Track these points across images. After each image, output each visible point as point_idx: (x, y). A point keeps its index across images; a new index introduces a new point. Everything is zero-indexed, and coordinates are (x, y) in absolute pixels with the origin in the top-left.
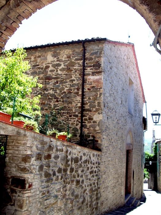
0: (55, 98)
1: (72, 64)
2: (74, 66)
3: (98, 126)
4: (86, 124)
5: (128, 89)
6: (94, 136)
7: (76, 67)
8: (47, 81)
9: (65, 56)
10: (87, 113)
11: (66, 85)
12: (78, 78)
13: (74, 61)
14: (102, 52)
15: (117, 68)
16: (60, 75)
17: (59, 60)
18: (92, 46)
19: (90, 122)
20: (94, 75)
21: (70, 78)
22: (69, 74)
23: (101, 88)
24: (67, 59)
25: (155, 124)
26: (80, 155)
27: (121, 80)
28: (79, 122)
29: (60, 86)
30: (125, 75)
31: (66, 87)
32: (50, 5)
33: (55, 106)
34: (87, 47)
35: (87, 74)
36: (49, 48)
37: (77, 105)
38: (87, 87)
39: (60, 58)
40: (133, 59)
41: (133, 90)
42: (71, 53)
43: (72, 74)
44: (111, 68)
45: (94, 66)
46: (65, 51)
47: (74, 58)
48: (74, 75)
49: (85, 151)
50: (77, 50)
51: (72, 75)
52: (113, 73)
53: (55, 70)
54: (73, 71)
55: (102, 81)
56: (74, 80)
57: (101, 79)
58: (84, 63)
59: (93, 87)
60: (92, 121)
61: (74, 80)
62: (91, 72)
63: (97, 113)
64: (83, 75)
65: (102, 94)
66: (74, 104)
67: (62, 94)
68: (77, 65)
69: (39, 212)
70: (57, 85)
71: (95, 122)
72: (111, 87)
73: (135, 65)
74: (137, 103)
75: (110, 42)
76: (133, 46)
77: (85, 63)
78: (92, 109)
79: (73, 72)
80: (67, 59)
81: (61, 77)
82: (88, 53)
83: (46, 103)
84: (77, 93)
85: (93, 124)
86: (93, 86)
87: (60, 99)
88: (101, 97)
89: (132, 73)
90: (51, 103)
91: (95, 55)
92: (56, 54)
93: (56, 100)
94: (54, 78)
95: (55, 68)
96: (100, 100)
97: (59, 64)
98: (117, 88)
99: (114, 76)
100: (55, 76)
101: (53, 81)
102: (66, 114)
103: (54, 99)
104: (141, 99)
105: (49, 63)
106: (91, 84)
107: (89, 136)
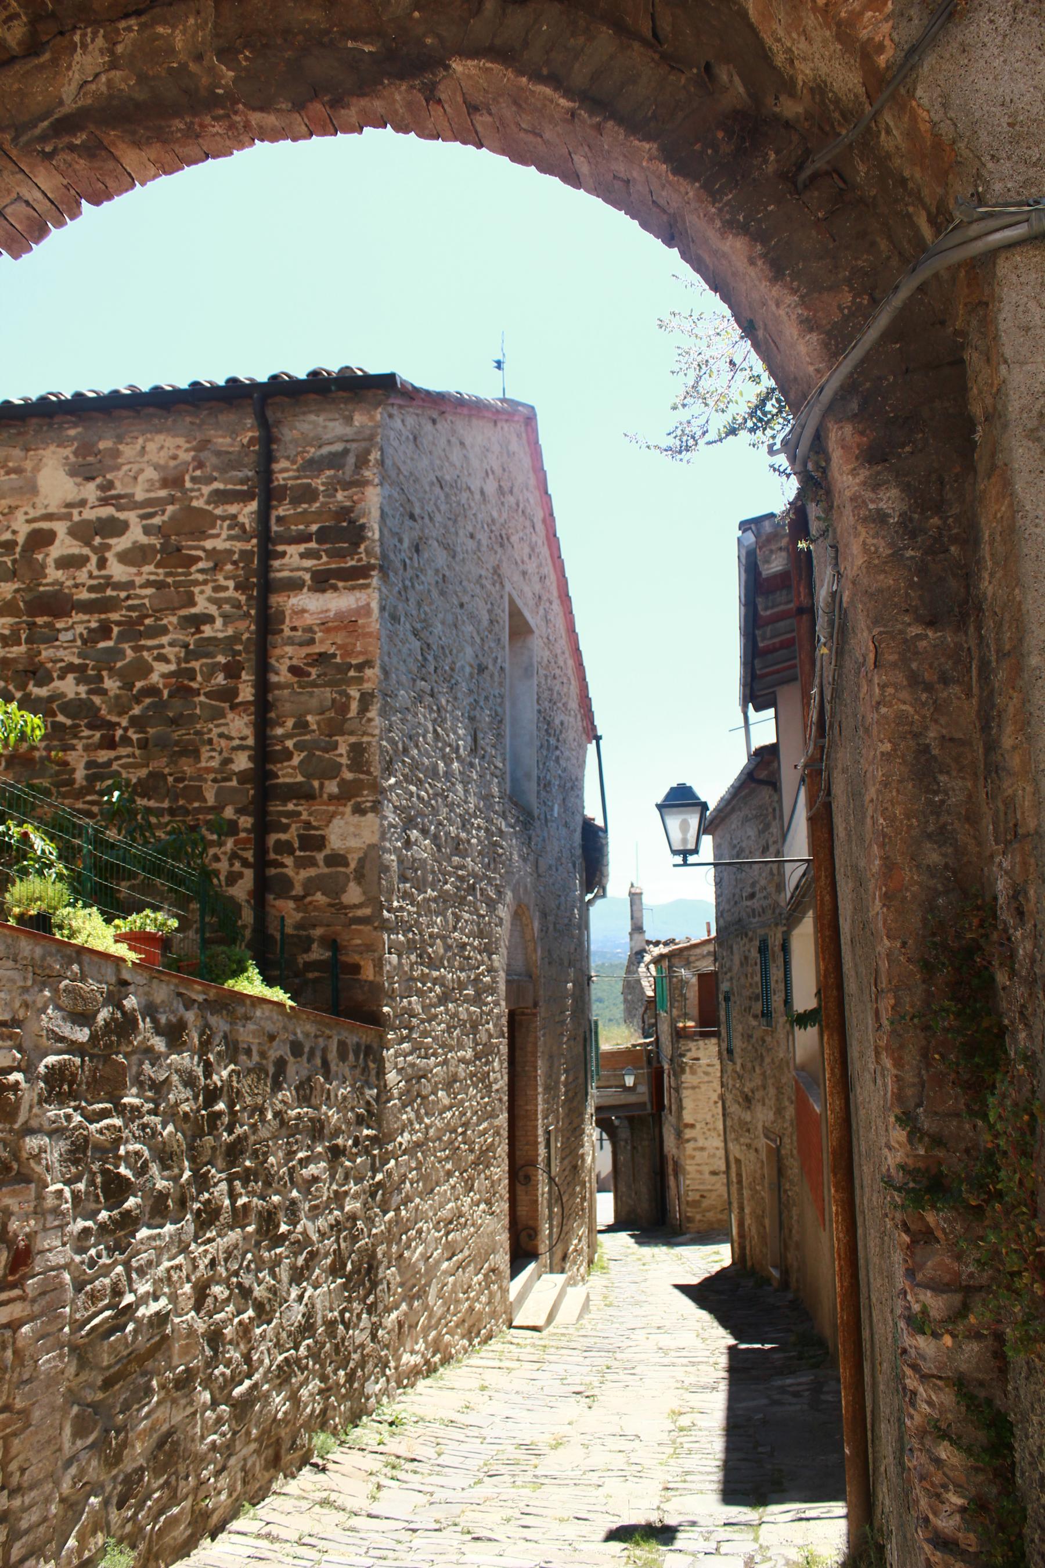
0: (90, 727)
1: (197, 524)
2: (204, 535)
3: (359, 883)
4: (285, 875)
5: (507, 666)
6: (335, 941)
7: (219, 541)
8: (40, 621)
9: (150, 473)
10: (290, 807)
11: (162, 646)
12: (233, 607)
13: (208, 503)
14: (368, 452)
15: (447, 547)
16: (118, 586)
17: (113, 497)
18: (312, 417)
19: (312, 863)
20: (323, 591)
21: (180, 608)
22: (177, 584)
23: (368, 664)
24: (163, 493)
25: (679, 859)
26: (273, 1054)
27: (471, 616)
28: (245, 863)
29: (122, 653)
30: (488, 584)
31: (163, 658)
32: (164, 181)
33: (97, 772)
34: (278, 422)
35: (281, 579)
36: (50, 425)
37: (227, 761)
38: (286, 656)
39: (117, 484)
40: (527, 494)
41: (528, 672)
42: (186, 456)
43: (196, 583)
44: (417, 550)
45: (322, 536)
46: (151, 447)
47: (206, 490)
48: (208, 589)
49: (299, 1031)
50: (222, 441)
51: (196, 590)
52: (430, 572)
53: (87, 559)
54: (201, 565)
55: (374, 623)
56: (209, 619)
57: (367, 610)
58: (263, 516)
59: (322, 659)
60: (320, 857)
61: (209, 619)
62: (306, 570)
63: (348, 809)
64: (263, 586)
65: (372, 695)
66: (210, 760)
67: (138, 702)
68: (223, 529)
69: (75, 1409)
70: (102, 645)
71: (337, 860)
72: (420, 658)
73: (540, 527)
74: (553, 741)
75: (412, 395)
76: (529, 419)
77: (273, 520)
78: (316, 784)
79: (201, 571)
80: (163, 493)
81: (128, 598)
82: (288, 458)
83: (37, 754)
84: (228, 695)
85: (326, 870)
86: (320, 654)
87: (126, 729)
88: (369, 715)
89: (524, 573)
90: (71, 757)
91: (329, 473)
92: (90, 459)
93: (98, 735)
94: (87, 607)
95: (88, 543)
96: (365, 734)
97: (112, 520)
98: (448, 660)
99: (435, 593)
100: (93, 596)
101: (81, 623)
102: (166, 819)
103: (86, 733)
104: (572, 719)
105: (49, 517)
106: (311, 642)
107: (306, 945)
